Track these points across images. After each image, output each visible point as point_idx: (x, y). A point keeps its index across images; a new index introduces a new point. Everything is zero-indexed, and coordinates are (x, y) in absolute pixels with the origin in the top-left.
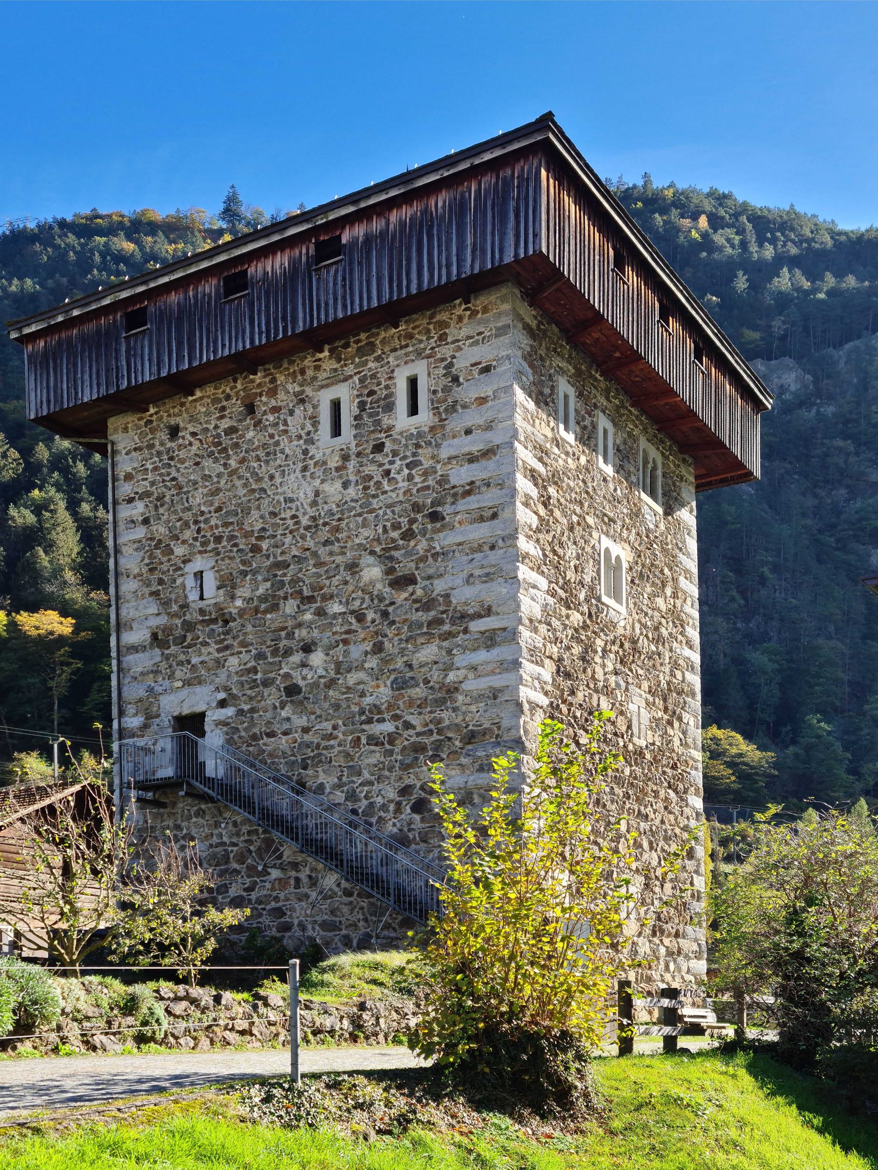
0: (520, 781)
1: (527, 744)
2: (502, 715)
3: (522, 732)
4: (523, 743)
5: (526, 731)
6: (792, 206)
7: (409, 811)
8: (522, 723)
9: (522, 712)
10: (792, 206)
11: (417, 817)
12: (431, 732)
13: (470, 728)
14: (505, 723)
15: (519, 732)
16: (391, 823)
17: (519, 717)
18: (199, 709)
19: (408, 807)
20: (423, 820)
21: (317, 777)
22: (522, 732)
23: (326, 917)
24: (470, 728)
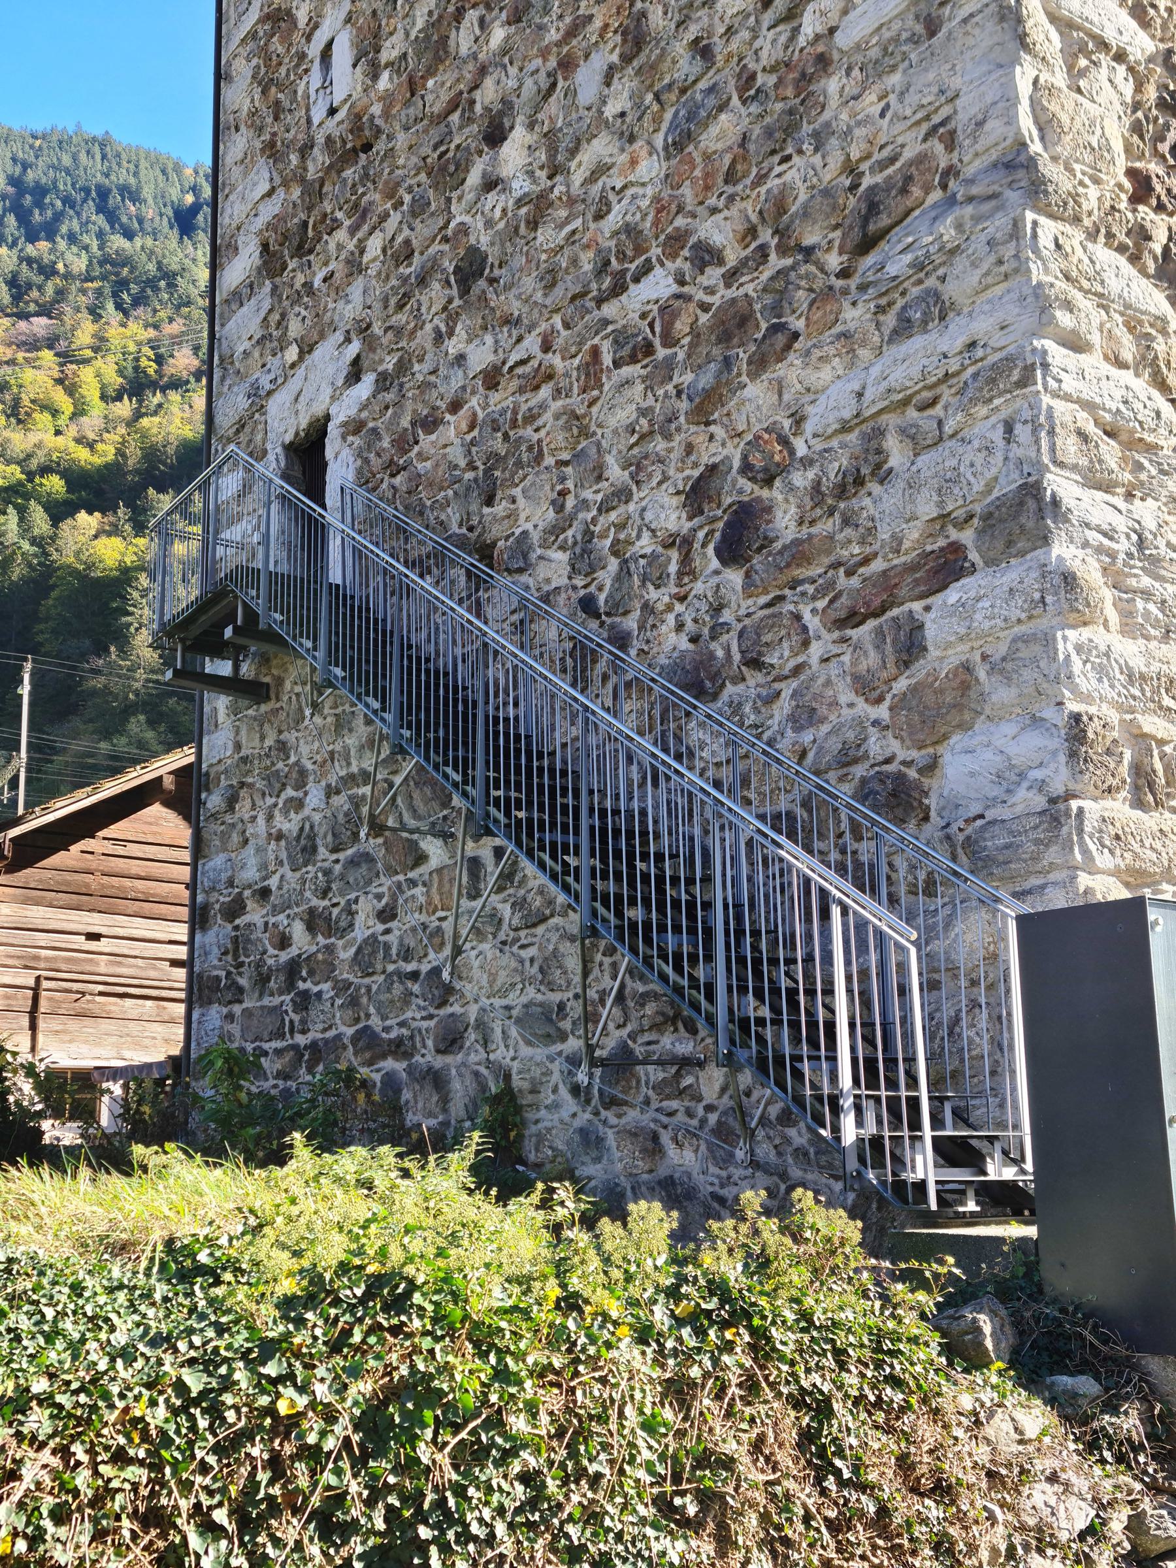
0: (1027, 321)
1: (1050, 170)
2: (956, 82)
3: (1026, 122)
4: (1031, 164)
5: (1046, 125)
6: (78, 125)
7: (715, 563)
8: (1024, 88)
9: (1022, 41)
10: (78, 125)
11: (735, 577)
12: (763, 253)
13: (867, 182)
14: (967, 109)
15: (1011, 119)
16: (671, 619)
17: (1007, 66)
18: (318, 409)
19: (710, 550)
20: (750, 587)
21: (512, 516)
22: (1026, 122)
23: (531, 993)
24: (867, 182)
